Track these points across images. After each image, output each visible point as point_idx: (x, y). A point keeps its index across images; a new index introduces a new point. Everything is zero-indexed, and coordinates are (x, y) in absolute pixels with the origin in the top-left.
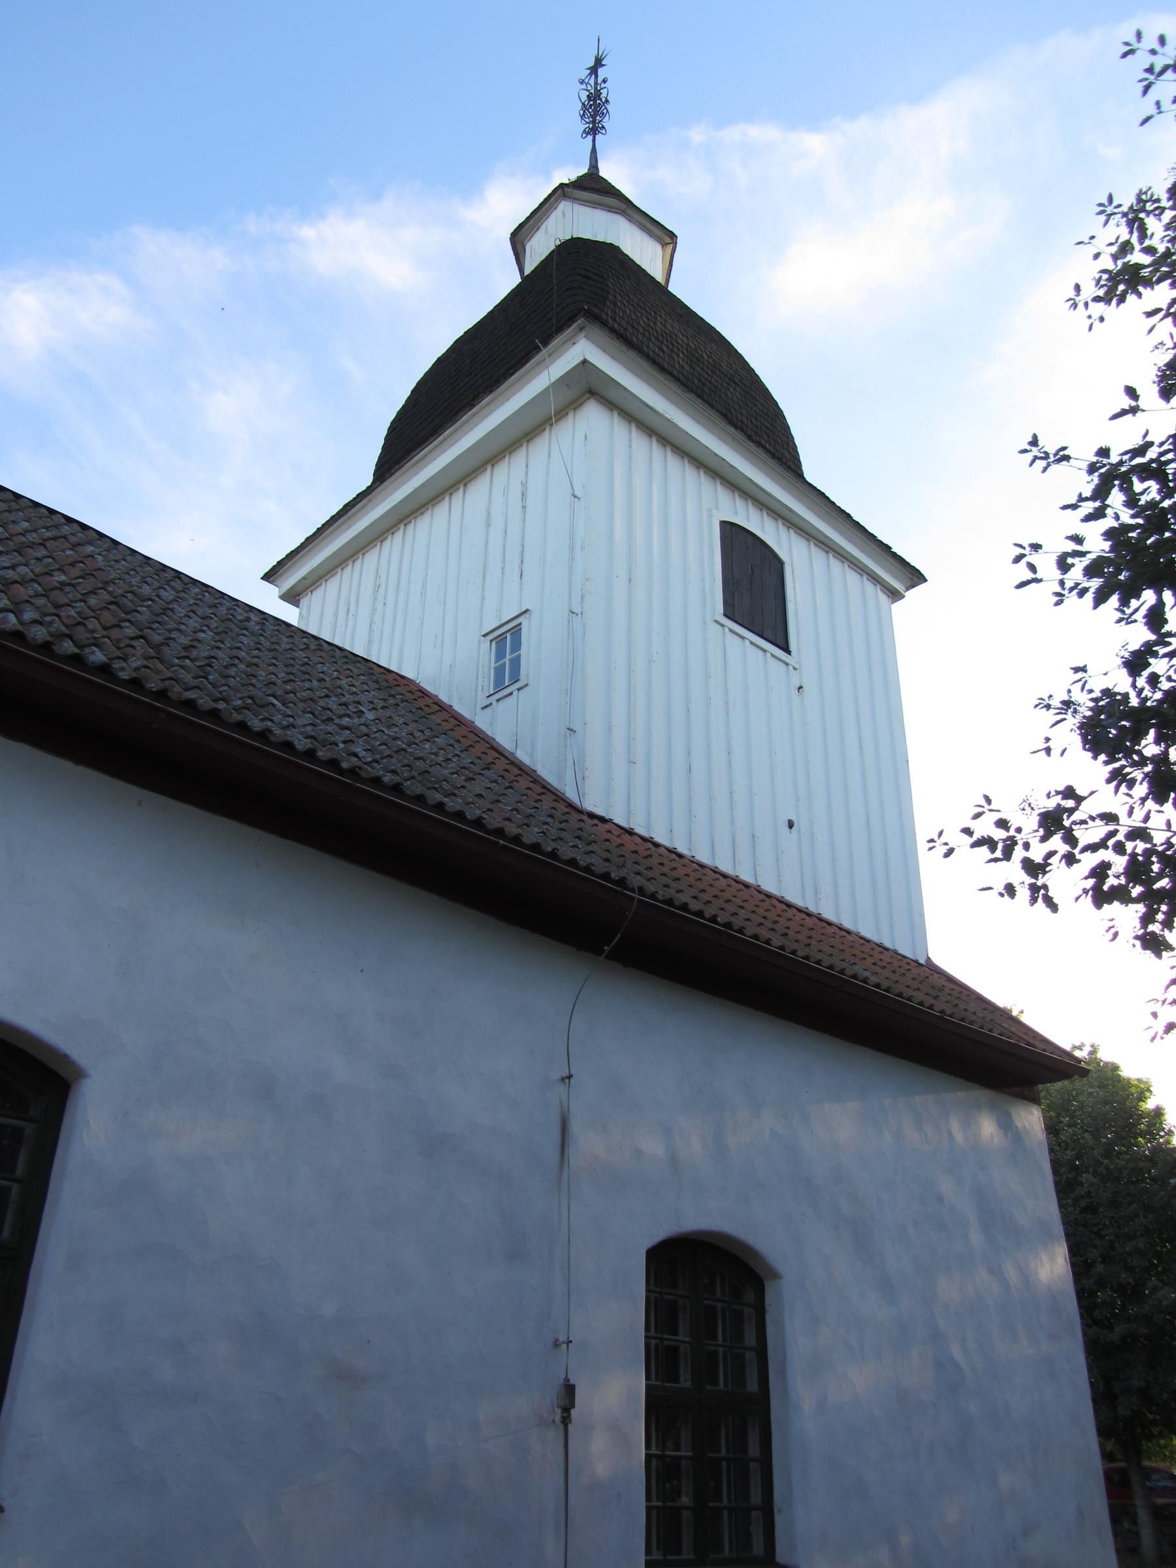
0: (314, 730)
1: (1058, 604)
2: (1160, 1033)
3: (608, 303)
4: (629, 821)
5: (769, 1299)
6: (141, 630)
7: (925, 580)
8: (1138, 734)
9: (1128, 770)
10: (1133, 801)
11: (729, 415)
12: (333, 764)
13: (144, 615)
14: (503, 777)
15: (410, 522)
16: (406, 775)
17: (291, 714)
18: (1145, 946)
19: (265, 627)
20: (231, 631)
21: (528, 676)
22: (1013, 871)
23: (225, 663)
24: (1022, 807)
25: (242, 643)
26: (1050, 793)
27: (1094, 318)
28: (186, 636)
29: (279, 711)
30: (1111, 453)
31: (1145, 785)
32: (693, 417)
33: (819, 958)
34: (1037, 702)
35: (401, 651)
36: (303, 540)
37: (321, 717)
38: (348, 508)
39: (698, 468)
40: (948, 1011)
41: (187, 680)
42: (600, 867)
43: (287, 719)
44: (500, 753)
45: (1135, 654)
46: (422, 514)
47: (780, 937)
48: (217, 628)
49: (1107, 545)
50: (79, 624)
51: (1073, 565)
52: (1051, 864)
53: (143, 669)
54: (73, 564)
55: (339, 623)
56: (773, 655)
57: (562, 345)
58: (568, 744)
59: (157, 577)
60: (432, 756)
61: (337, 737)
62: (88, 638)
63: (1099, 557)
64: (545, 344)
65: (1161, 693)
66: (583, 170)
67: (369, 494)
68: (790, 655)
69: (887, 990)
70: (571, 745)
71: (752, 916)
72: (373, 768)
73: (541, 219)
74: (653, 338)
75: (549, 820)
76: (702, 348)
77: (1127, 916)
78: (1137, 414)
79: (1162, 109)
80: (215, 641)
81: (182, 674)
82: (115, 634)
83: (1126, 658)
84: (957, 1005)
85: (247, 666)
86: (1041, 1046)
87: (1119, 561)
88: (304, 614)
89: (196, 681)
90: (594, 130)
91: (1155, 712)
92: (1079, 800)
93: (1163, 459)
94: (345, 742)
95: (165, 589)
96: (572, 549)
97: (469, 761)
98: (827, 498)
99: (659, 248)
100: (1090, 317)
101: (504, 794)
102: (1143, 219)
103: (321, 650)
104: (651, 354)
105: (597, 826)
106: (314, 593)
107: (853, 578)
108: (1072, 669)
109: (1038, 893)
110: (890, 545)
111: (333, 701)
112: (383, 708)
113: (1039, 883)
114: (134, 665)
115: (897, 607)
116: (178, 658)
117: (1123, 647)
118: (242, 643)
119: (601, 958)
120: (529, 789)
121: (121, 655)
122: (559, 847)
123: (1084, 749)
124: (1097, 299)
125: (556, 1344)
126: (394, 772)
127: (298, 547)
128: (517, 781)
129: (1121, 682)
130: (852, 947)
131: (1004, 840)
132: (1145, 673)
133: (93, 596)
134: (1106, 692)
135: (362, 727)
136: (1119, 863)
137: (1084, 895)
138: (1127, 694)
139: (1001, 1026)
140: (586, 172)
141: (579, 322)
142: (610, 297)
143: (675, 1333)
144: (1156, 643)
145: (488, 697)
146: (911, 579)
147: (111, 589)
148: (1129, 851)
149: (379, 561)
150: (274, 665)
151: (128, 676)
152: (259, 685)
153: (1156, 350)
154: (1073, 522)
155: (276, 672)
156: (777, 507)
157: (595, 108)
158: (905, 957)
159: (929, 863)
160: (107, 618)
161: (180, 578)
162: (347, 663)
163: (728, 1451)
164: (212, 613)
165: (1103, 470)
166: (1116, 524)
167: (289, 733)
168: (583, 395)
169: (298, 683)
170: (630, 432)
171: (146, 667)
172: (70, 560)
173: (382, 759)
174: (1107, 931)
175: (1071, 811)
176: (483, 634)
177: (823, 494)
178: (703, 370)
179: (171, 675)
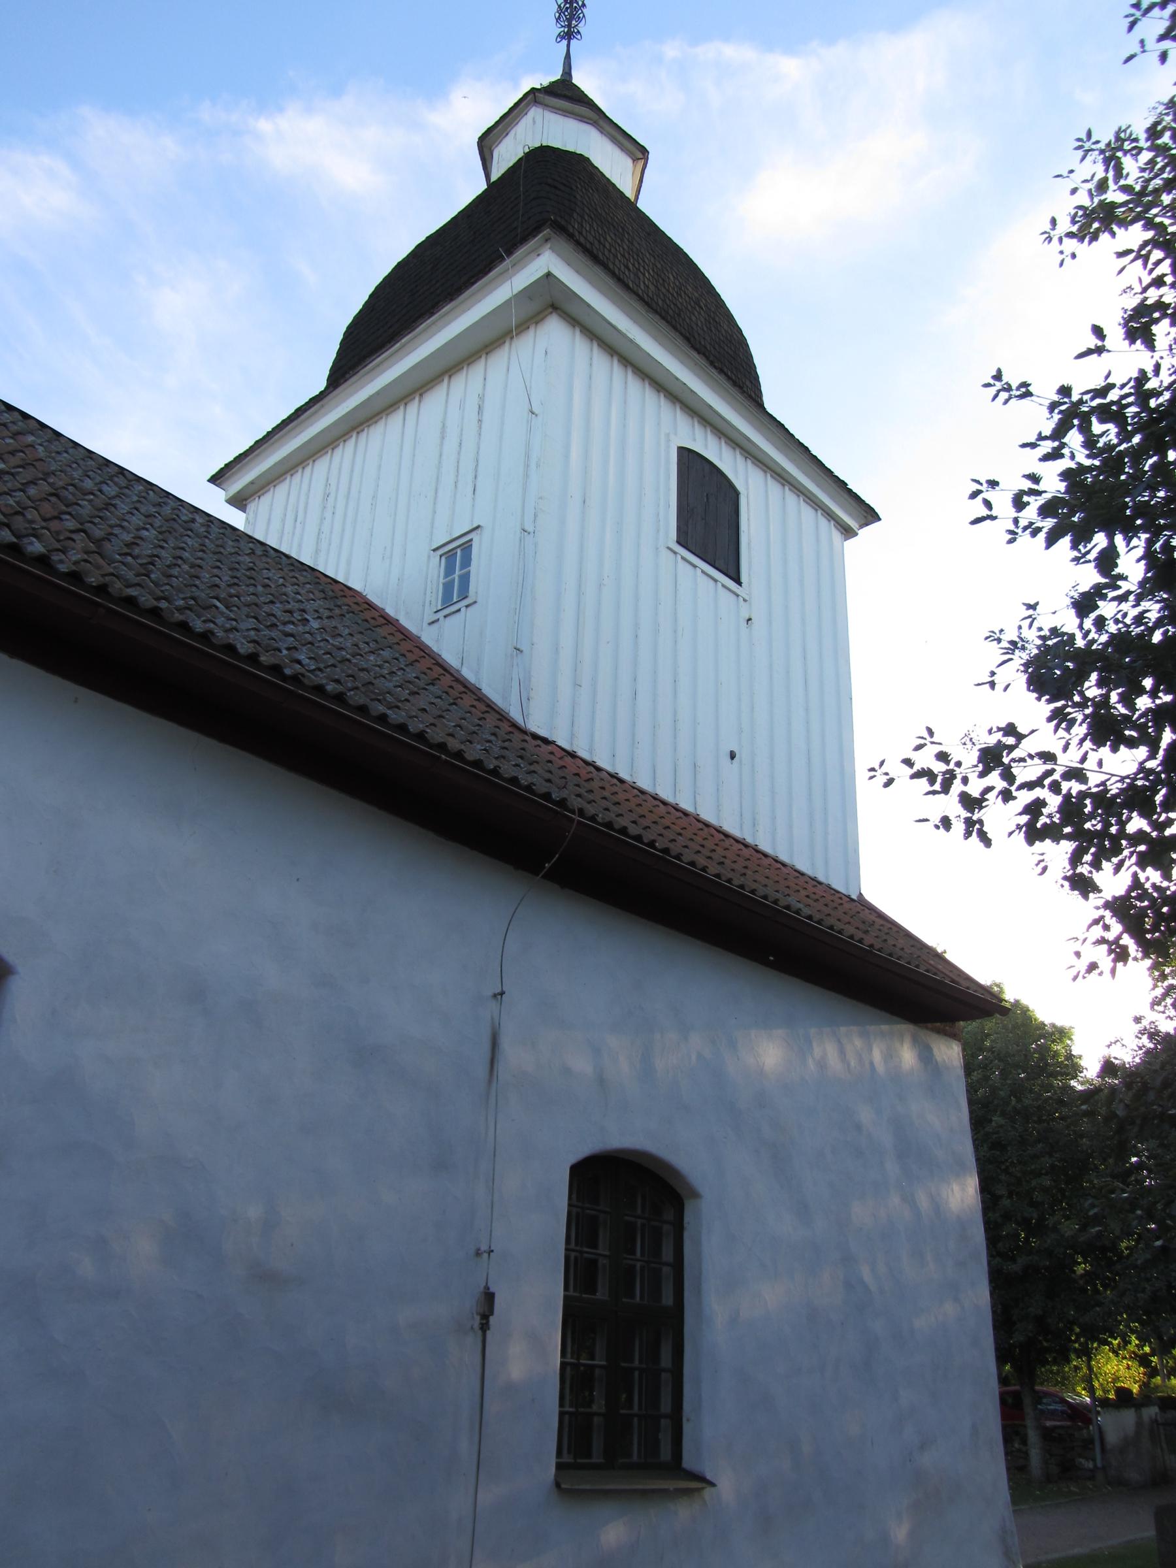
0: (257, 636)
1: (1010, 541)
2: (1083, 972)
3: (575, 215)
4: (572, 744)
5: (688, 1217)
6: (82, 524)
7: (880, 519)
8: (1083, 676)
9: (1069, 710)
10: (1070, 737)
11: (692, 339)
12: (276, 669)
13: (86, 509)
14: (447, 693)
15: (363, 430)
16: (349, 685)
17: (233, 617)
18: (1073, 887)
19: (210, 529)
20: (175, 531)
21: (476, 593)
22: (950, 805)
23: (168, 563)
24: (963, 741)
25: (186, 544)
26: (991, 729)
27: (1065, 254)
28: (129, 533)
29: (222, 613)
30: (1073, 392)
31: (1085, 726)
32: (655, 338)
33: (754, 887)
34: (988, 634)
35: (349, 563)
36: (252, 443)
37: (265, 622)
38: (300, 413)
39: (659, 391)
40: (877, 946)
41: (128, 577)
42: (541, 787)
43: (230, 622)
44: (445, 670)
45: (1084, 595)
46: (376, 422)
47: (717, 866)
48: (161, 527)
49: (1062, 486)
50: (17, 513)
51: (1028, 503)
52: (987, 800)
53: (82, 563)
54: (13, 453)
55: (286, 532)
56: (723, 586)
57: (526, 256)
58: (515, 664)
59: (100, 472)
60: (377, 668)
61: (280, 643)
62: (26, 529)
63: (1055, 498)
64: (510, 253)
65: (1107, 635)
66: (556, 76)
67: (322, 399)
68: (741, 586)
69: (819, 922)
70: (517, 665)
71: (690, 844)
72: (316, 676)
73: (512, 123)
74: (619, 255)
75: (493, 738)
76: (669, 269)
77: (1059, 852)
78: (1102, 355)
79: (1146, 48)
80: (159, 540)
81: (123, 571)
82: (54, 526)
83: (1075, 599)
84: (885, 940)
85: (191, 567)
86: (965, 983)
87: (1073, 502)
88: (251, 519)
89: (138, 578)
90: (569, 35)
91: (1100, 655)
92: (1020, 737)
93: (1124, 402)
94: (288, 649)
95: (107, 484)
96: (527, 466)
97: (414, 675)
98: (787, 430)
99: (629, 162)
100: (1061, 252)
101: (448, 710)
102: (1120, 158)
103: (267, 556)
104: (617, 271)
105: (540, 747)
106: (262, 498)
107: (807, 512)
108: (1024, 604)
109: (973, 827)
110: (846, 481)
111: (278, 608)
112: (329, 617)
113: (975, 818)
114: (74, 558)
115: (850, 544)
116: (120, 555)
117: (1073, 587)
118: (186, 544)
119: (538, 878)
120: (473, 706)
121: (60, 547)
122: (501, 765)
123: (1029, 689)
124: (1070, 235)
125: (478, 1253)
126: (338, 681)
127: (247, 450)
128: (462, 698)
129: (1069, 622)
130: (786, 879)
131: (944, 773)
132: (1093, 616)
133: (33, 486)
134: (1054, 631)
135: (307, 635)
136: (1054, 802)
137: (1018, 830)
138: (1073, 635)
139: (928, 963)
140: (559, 78)
141: (545, 232)
142: (578, 210)
143: (595, 1247)
144: (1106, 586)
145: (436, 612)
146: (865, 517)
147: (51, 480)
148: (1064, 792)
149: (329, 469)
150: (218, 567)
151: (68, 568)
152: (202, 587)
153: (1124, 294)
154: (1031, 461)
155: (220, 575)
156: (734, 436)
157: (572, 12)
158: (838, 892)
159: (867, 792)
160: (47, 509)
161: (124, 475)
162: (293, 570)
163: (641, 1361)
164: (156, 512)
165: (1063, 408)
166: (1073, 465)
167: (231, 636)
168: (546, 309)
169: (243, 587)
170: (592, 350)
171: (86, 561)
172: (10, 448)
173: (325, 668)
174: (1037, 865)
175: (1011, 748)
176: (434, 547)
177: (782, 426)
178: (668, 291)
179: (112, 570)
